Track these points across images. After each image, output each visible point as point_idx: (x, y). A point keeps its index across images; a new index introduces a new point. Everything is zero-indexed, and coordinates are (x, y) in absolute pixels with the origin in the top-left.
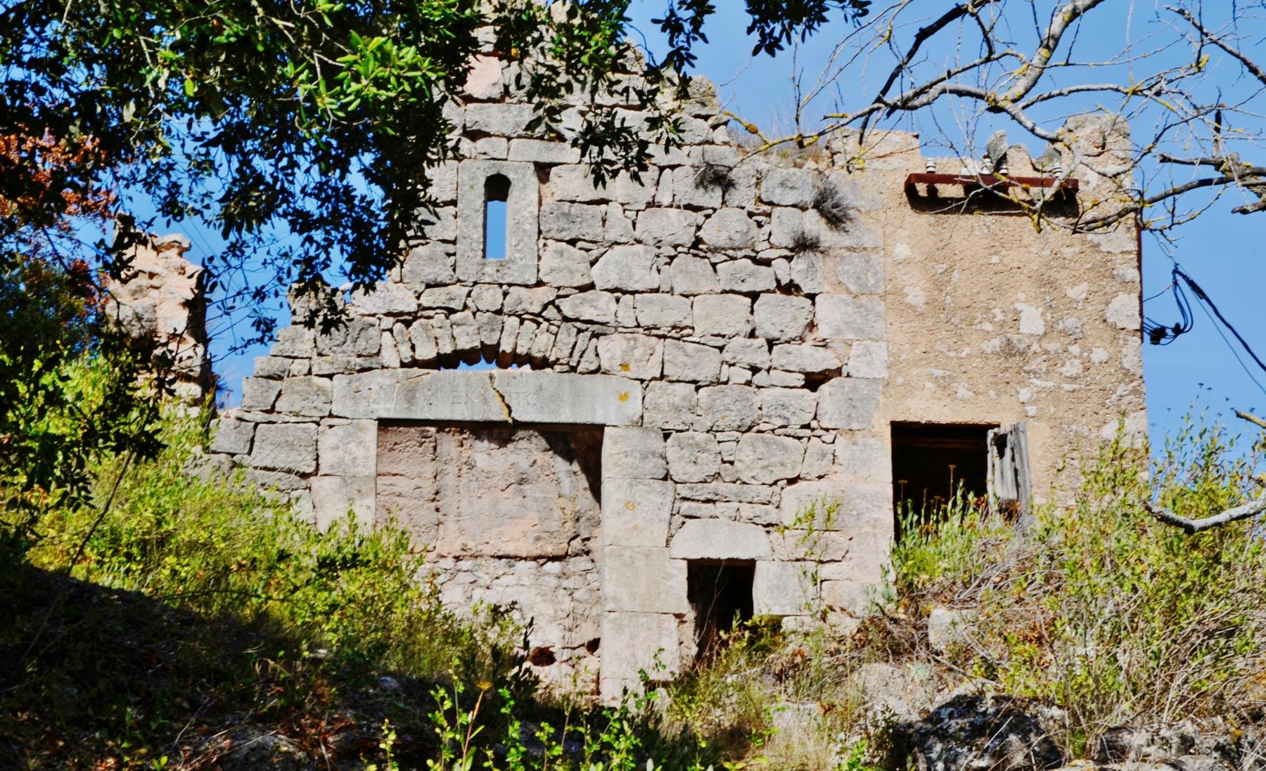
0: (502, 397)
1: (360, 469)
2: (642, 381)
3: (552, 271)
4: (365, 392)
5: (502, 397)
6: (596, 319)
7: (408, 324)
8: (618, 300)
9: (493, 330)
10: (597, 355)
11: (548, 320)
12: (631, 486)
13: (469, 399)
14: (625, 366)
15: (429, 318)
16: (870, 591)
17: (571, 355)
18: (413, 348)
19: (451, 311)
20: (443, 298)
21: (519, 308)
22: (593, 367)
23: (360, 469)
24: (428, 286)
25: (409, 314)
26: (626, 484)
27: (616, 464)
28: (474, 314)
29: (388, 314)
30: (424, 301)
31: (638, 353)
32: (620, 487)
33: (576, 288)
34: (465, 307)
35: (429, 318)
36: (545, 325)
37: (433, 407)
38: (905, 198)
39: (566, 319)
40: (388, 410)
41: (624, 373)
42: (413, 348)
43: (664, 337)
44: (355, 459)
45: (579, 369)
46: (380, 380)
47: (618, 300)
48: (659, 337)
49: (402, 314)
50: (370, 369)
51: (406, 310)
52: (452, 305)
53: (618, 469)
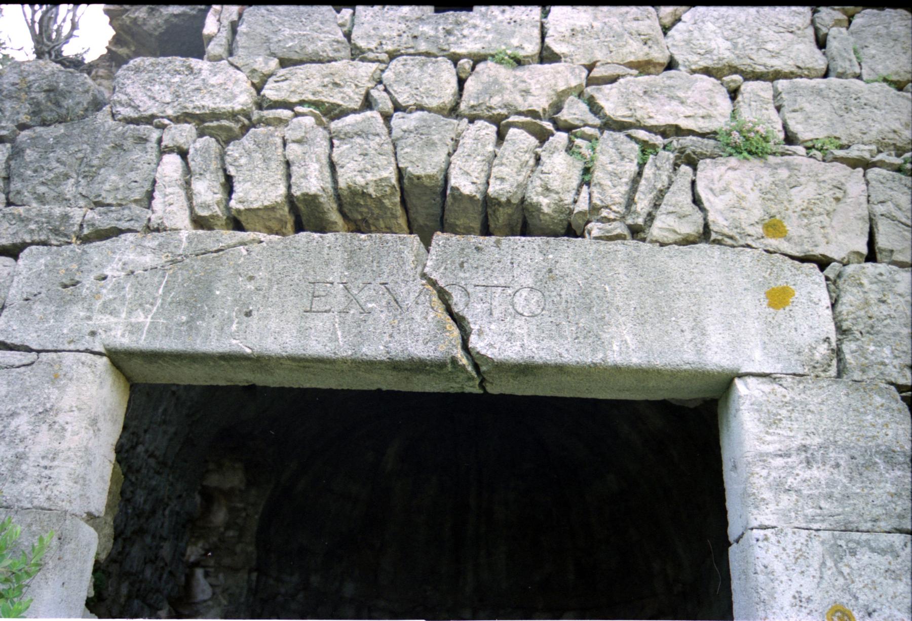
0: (444, 296)
1: (27, 487)
2: (823, 263)
3: (574, 33)
4: (88, 282)
5: (444, 296)
6: (684, 124)
7: (227, 138)
8: (734, 94)
9: (430, 144)
10: (696, 201)
11: (568, 128)
12: (837, 553)
13: (352, 299)
14: (773, 227)
15: (280, 121)
16: (797, 595)
17: (630, 202)
18: (229, 185)
19: (333, 112)
20: (315, 84)
21: (496, 101)
22: (690, 228)
23: (27, 487)
24: (284, 63)
25: (233, 115)
26: (817, 548)
27: (780, 487)
28: (387, 118)
29: (184, 117)
30: (270, 92)
31: (801, 196)
32: (800, 556)
33: (631, 65)
34: (368, 103)
35: (280, 121)
36: (561, 138)
37: (254, 321)
38: (27, 344)
39: (610, 125)
40: (134, 329)
41: (773, 243)
42: (229, 185)
43: (866, 165)
44: (20, 457)
45: (656, 231)
46: (131, 256)
47: (734, 94)
48: (854, 163)
49: (215, 115)
50: (116, 232)
51: (227, 106)
52: (335, 98)
53: (786, 501)
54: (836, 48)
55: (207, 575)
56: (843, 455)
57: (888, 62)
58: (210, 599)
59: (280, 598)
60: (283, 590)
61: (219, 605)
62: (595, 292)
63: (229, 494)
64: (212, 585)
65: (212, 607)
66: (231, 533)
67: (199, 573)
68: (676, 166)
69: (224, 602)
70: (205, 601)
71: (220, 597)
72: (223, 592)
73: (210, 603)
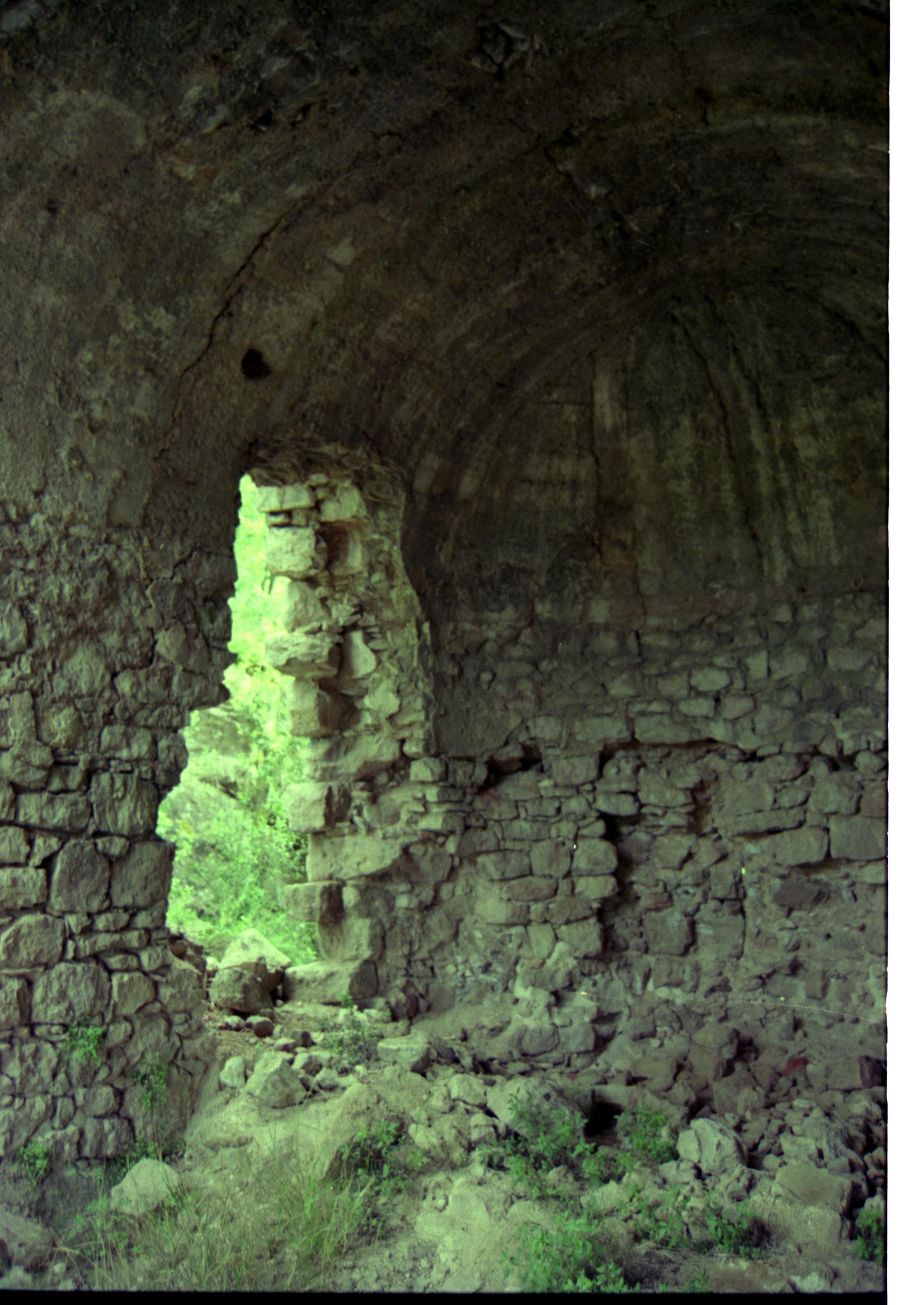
54: (349, 54)
55: (368, 638)
56: (63, 1037)
57: (107, 1124)
58: (375, 671)
59: (489, 647)
60: (492, 634)
61: (389, 676)
62: (736, 998)
63: (356, 524)
64: (374, 651)
65: (381, 680)
66: (376, 577)
67: (357, 637)
68: (20, 976)
69: (394, 671)
70: (369, 675)
71: (387, 665)
72: (390, 657)
73: (376, 675)
